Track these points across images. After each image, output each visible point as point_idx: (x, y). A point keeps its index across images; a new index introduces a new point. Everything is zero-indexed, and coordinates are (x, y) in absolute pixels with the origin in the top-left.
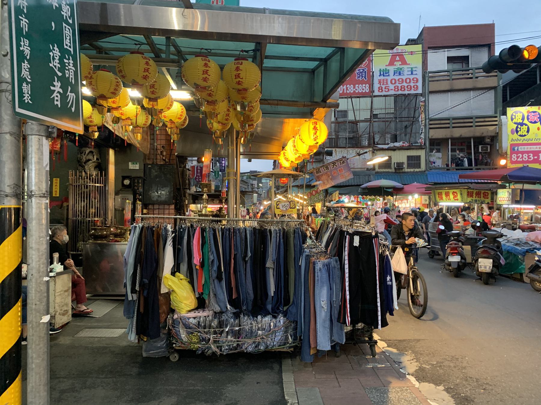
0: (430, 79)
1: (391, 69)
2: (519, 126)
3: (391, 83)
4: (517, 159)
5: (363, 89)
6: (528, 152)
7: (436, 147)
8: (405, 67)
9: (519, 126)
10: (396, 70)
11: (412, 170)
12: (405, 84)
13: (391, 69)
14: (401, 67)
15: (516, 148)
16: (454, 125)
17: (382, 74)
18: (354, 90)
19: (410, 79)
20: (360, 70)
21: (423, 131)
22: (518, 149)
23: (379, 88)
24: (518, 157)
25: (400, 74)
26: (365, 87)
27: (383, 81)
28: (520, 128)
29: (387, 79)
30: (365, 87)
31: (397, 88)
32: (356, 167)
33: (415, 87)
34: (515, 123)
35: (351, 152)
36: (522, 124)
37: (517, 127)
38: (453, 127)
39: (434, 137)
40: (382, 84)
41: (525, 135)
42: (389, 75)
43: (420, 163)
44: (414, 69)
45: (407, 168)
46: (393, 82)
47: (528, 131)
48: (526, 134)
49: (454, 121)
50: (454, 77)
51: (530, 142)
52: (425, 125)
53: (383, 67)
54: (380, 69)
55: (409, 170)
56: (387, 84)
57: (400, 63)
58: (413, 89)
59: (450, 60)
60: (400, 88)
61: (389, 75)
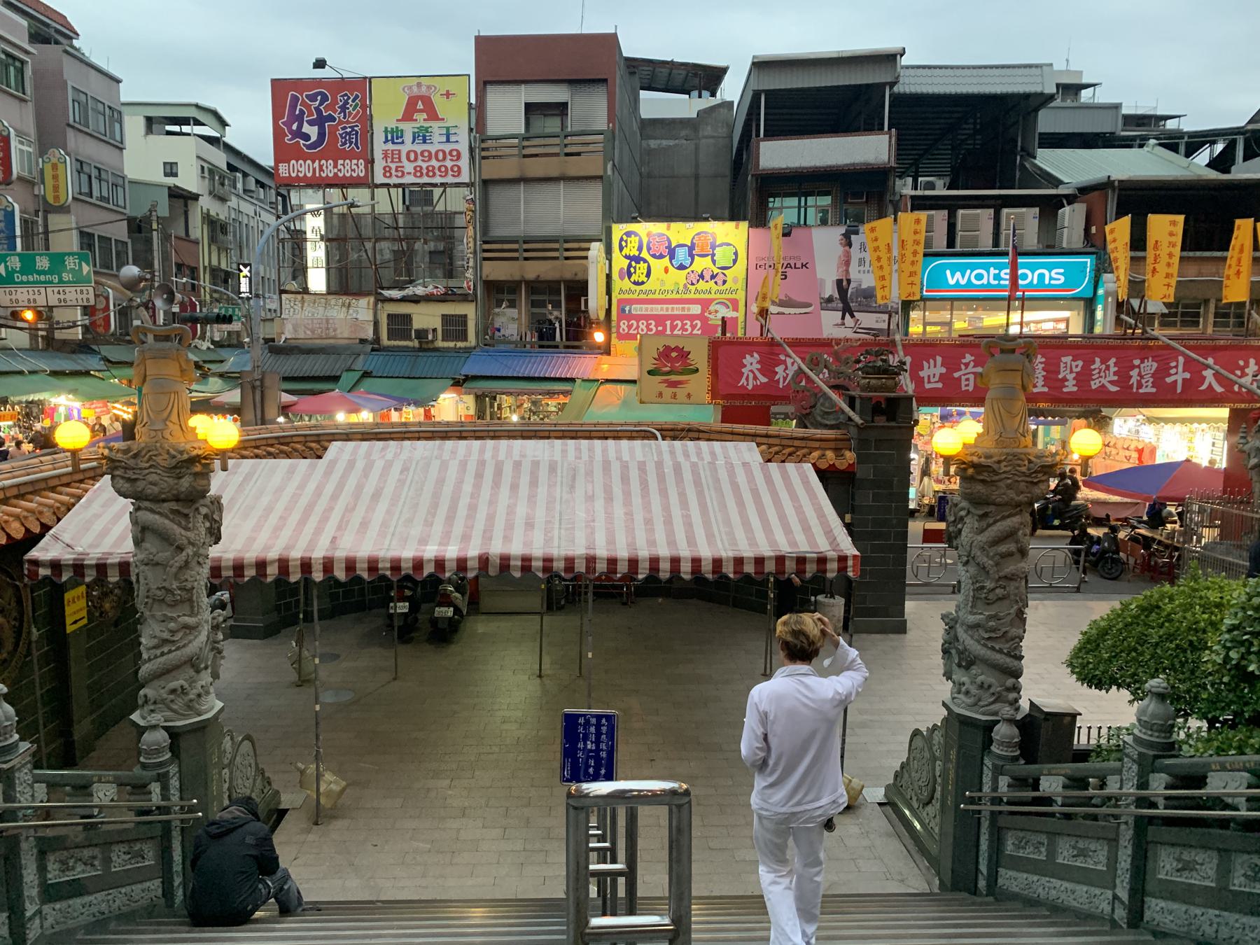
0: (484, 154)
1: (408, 128)
2: (633, 264)
3: (408, 159)
4: (693, 330)
5: (354, 170)
6: (647, 317)
7: (506, 296)
8: (435, 125)
9: (633, 264)
10: (416, 130)
11: (451, 344)
12: (434, 162)
13: (408, 128)
14: (426, 125)
15: (627, 309)
16: (556, 246)
17: (389, 138)
18: (336, 170)
19: (444, 152)
20: (345, 128)
21: (471, 264)
22: (630, 311)
23: (384, 168)
24: (630, 327)
25: (424, 142)
26: (357, 165)
27: (393, 154)
28: (635, 268)
29: (399, 151)
30: (357, 165)
31: (418, 171)
32: (340, 336)
33: (456, 169)
34: (627, 257)
35: (333, 302)
36: (638, 259)
37: (630, 266)
38: (526, 259)
39: (491, 278)
40: (389, 160)
41: (643, 283)
42: (403, 142)
43: (466, 331)
44: (452, 131)
45: (443, 340)
46: (412, 156)
47: (648, 275)
48: (645, 280)
49: (526, 246)
50: (557, 141)
51: (651, 296)
52: (475, 252)
53: (392, 125)
54: (386, 128)
55: (446, 344)
56: (400, 161)
57: (425, 116)
58: (450, 173)
59: (531, 109)
60: (425, 171)
61: (403, 142)
